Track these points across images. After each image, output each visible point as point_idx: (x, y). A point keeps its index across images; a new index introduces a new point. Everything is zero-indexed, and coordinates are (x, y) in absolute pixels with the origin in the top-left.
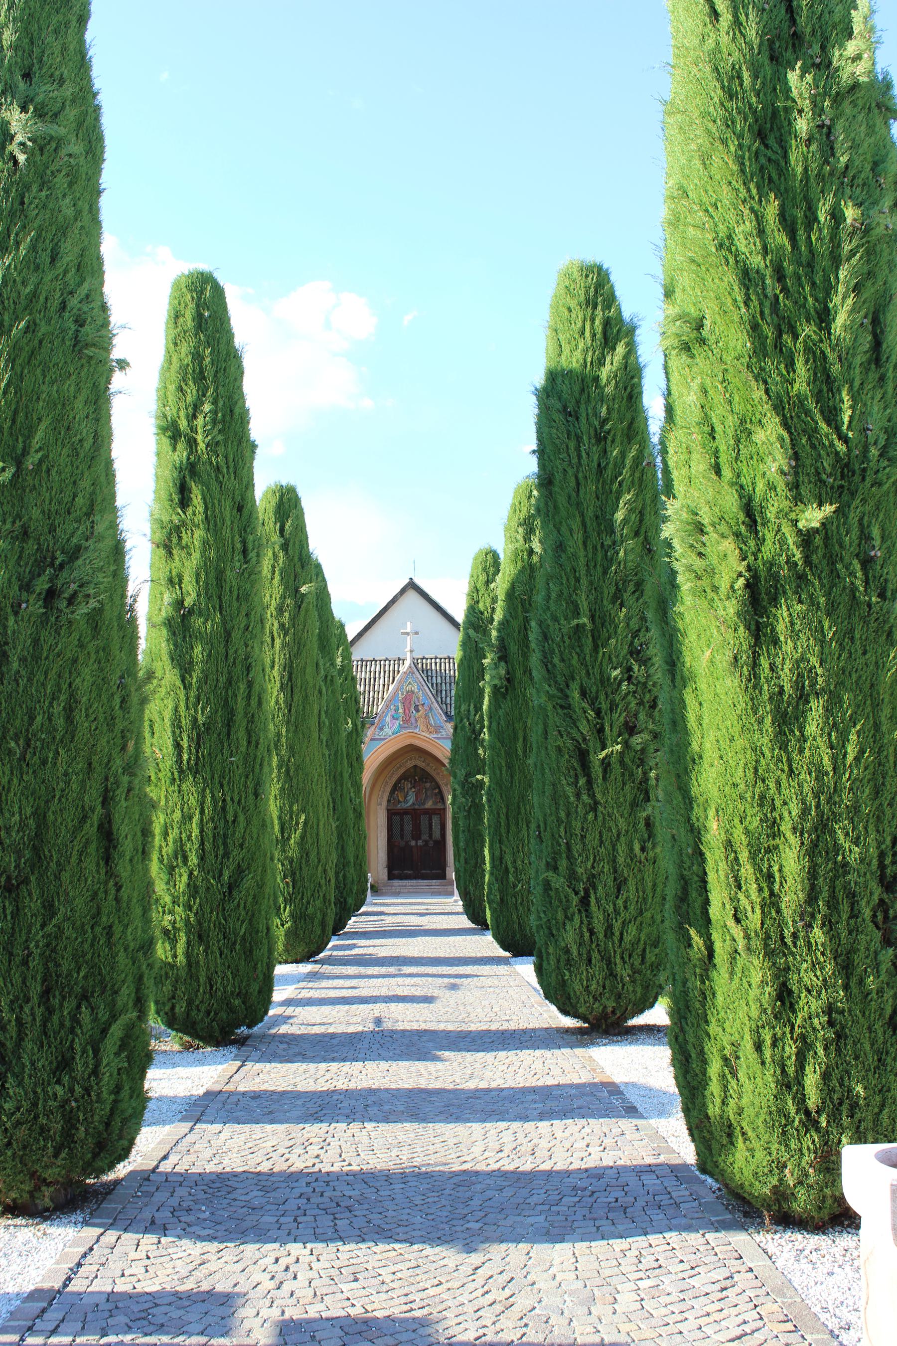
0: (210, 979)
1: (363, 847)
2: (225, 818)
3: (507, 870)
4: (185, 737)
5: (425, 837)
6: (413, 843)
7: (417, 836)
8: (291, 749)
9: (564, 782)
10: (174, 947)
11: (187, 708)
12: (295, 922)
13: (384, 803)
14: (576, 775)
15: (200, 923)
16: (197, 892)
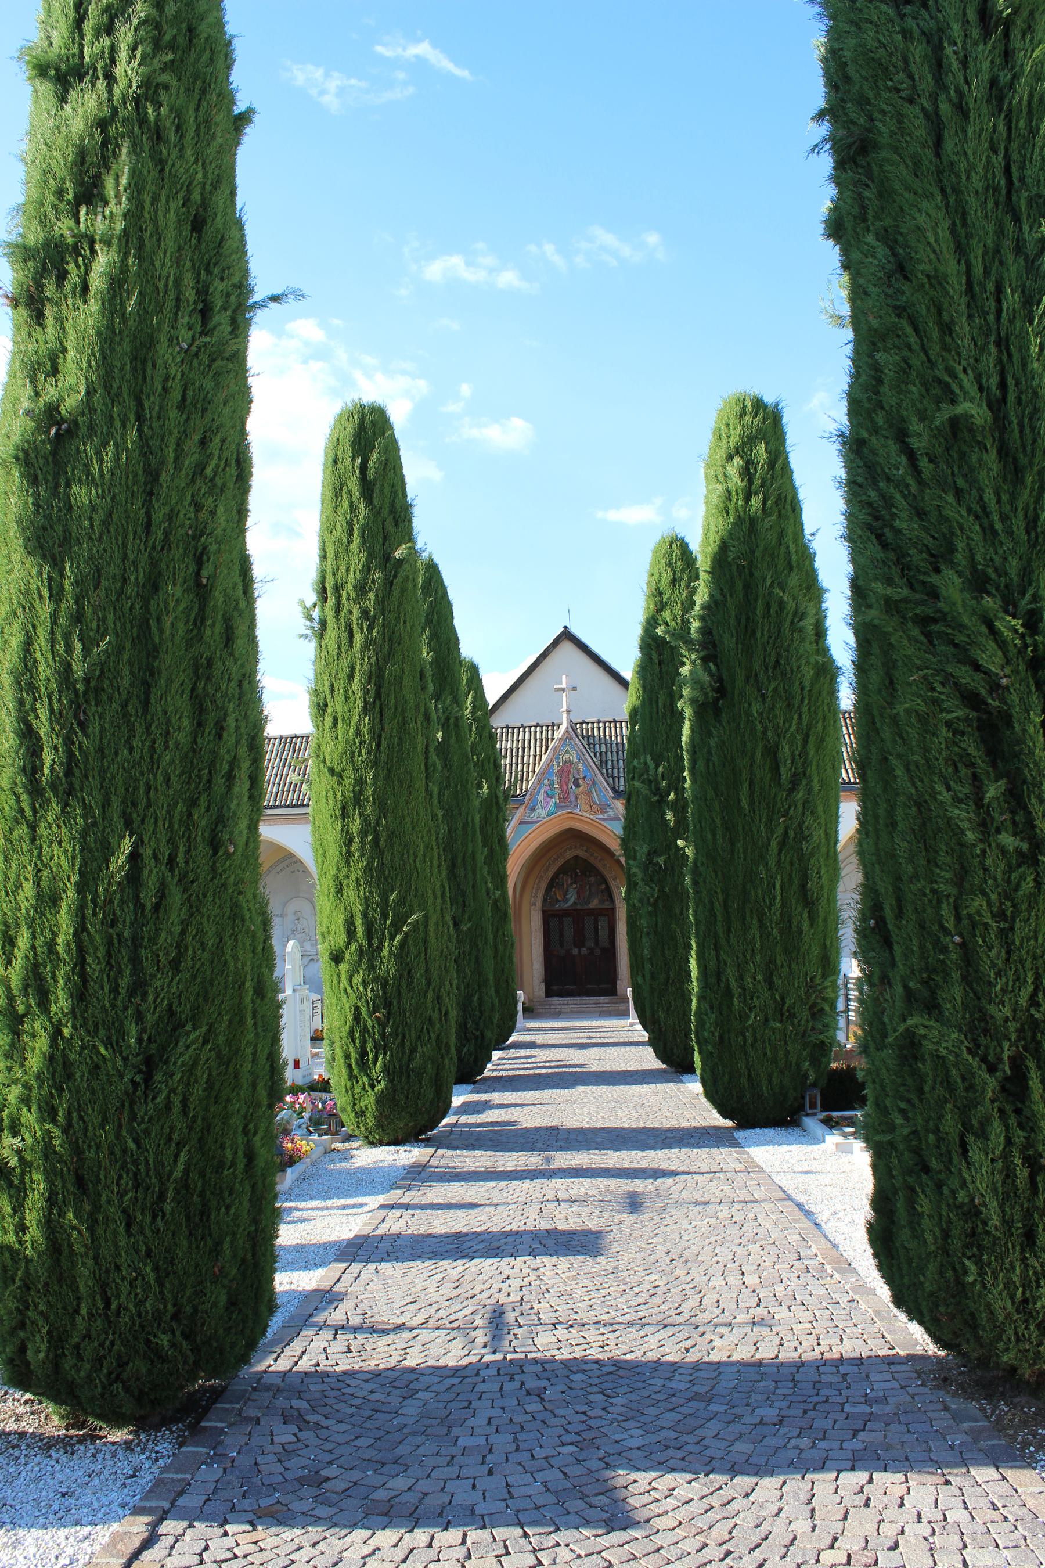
0: (104, 1286)
1: (510, 958)
2: (137, 898)
3: (728, 992)
4: (43, 712)
5: (590, 944)
6: (575, 951)
7: (579, 942)
8: (381, 806)
9: (945, 796)
10: (18, 1208)
11: (53, 642)
12: (391, 1081)
13: (539, 903)
14: (975, 776)
15: (77, 1150)
16: (70, 1076)
